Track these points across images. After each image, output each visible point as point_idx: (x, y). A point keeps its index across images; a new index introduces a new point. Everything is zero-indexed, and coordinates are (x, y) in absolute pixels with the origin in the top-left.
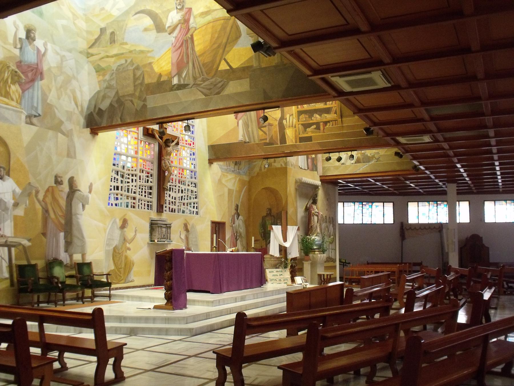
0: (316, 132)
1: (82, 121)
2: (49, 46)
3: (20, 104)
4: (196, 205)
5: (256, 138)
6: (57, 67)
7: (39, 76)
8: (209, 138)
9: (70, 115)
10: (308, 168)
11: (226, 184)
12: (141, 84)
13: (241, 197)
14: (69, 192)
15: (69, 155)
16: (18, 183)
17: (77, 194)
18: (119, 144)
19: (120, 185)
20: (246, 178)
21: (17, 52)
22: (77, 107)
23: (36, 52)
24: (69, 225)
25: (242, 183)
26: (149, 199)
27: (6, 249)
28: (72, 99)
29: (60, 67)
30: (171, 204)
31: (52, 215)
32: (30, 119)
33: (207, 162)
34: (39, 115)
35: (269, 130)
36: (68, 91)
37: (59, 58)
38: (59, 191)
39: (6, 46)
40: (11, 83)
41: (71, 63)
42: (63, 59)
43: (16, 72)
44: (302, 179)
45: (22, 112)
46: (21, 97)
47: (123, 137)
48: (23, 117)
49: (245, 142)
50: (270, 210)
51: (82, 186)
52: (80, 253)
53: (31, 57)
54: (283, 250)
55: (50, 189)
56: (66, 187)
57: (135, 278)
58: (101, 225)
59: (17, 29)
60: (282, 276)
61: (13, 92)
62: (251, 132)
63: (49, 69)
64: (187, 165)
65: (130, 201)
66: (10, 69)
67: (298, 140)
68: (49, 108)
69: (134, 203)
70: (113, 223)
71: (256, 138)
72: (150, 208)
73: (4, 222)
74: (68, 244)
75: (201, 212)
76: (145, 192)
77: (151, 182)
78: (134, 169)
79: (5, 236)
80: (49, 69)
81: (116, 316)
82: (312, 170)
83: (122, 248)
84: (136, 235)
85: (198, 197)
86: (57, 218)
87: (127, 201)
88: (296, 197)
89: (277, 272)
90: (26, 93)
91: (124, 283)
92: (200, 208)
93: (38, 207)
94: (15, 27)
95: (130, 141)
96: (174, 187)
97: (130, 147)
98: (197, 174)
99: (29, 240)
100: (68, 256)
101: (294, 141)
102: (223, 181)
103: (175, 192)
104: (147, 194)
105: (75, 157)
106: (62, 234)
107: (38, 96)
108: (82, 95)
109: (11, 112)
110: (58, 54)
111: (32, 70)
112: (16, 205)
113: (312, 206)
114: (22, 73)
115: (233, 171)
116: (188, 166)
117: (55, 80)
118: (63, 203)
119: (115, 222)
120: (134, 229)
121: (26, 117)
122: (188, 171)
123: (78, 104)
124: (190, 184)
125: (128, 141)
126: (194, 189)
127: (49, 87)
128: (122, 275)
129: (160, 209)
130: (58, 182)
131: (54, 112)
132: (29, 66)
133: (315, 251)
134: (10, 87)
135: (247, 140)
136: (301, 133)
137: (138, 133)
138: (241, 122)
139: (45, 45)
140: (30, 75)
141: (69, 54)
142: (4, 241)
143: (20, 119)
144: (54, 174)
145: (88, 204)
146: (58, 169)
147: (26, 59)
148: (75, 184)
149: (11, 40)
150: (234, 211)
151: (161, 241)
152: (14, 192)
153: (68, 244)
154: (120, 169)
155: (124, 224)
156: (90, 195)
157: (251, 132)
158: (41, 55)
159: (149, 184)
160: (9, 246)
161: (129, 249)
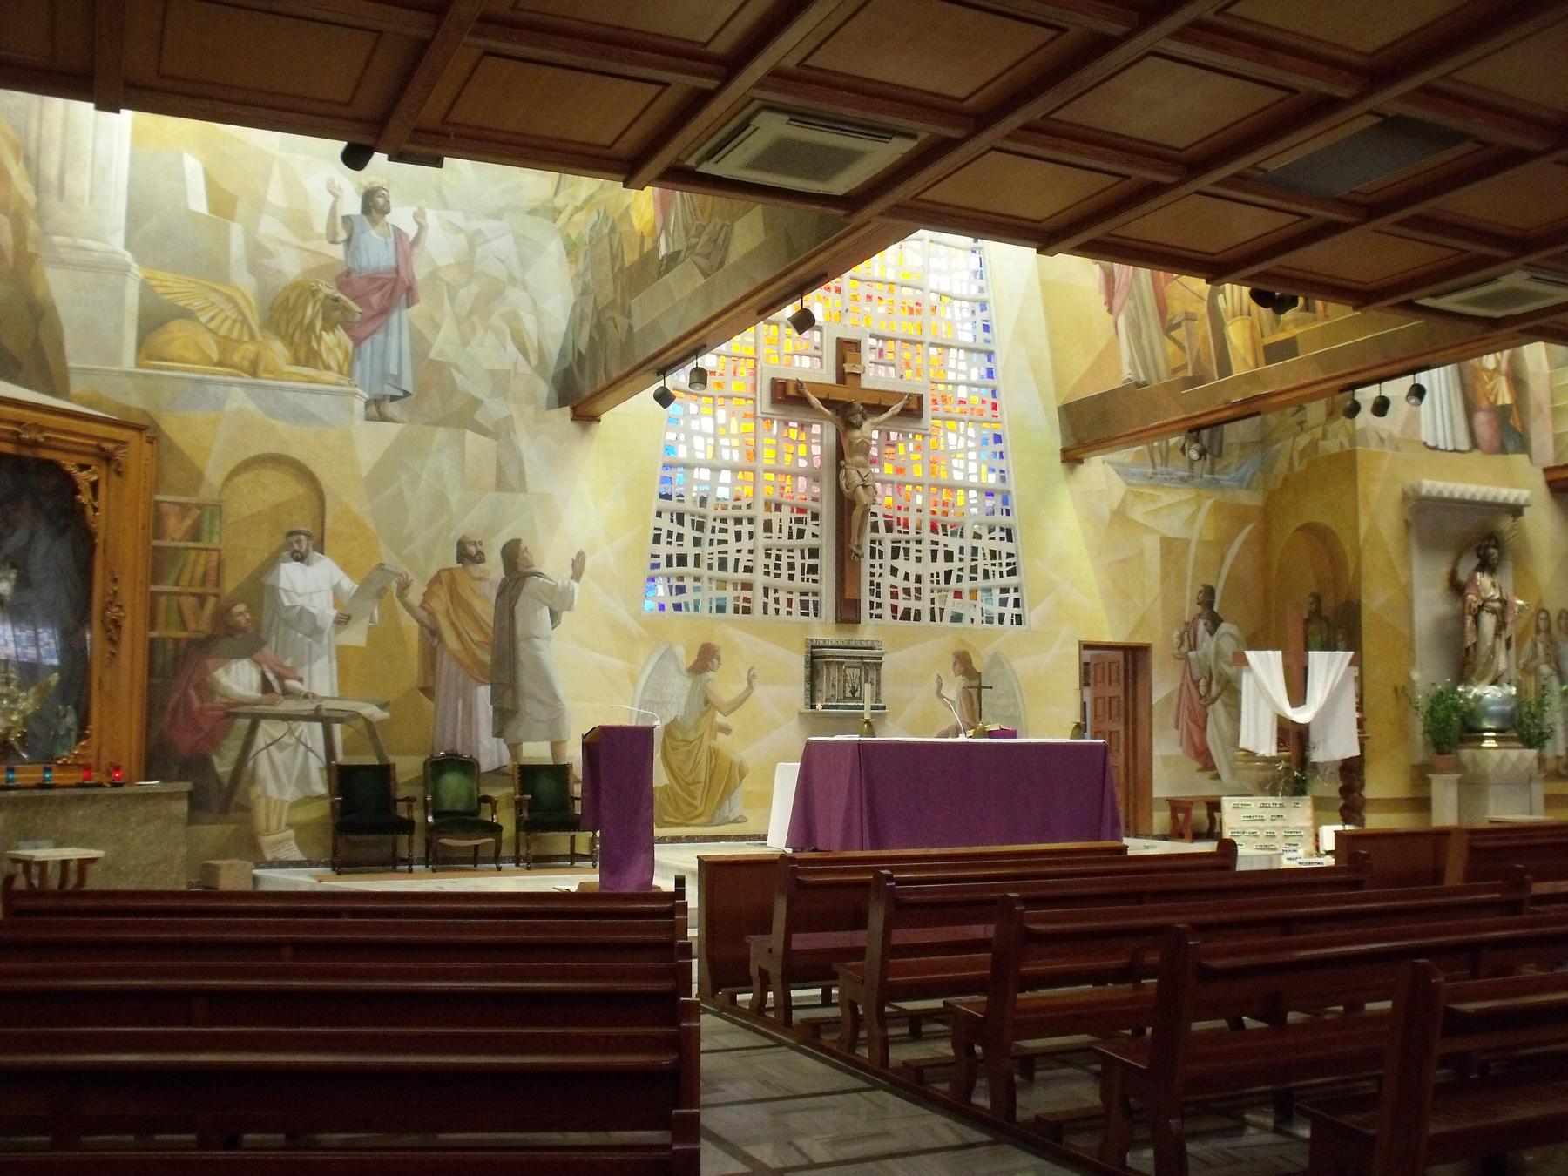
0: (1305, 322)
1: (543, 389)
2: (431, 217)
3: (350, 374)
4: (1012, 596)
5: (1162, 367)
6: (458, 264)
7: (404, 298)
8: (1058, 384)
9: (501, 382)
10: (1475, 444)
11: (1152, 524)
12: (621, 269)
13: (1229, 561)
14: (504, 581)
15: (501, 484)
16: (346, 567)
17: (532, 584)
18: (682, 437)
19: (689, 549)
20: (1251, 499)
21: (338, 252)
22: (525, 354)
23: (391, 240)
24: (506, 669)
25: (1235, 516)
26: (809, 586)
27: (318, 727)
28: (509, 338)
29: (467, 265)
30: (901, 595)
31: (451, 641)
32: (377, 409)
33: (1058, 458)
34: (406, 394)
35: (1190, 335)
36: (496, 320)
37: (462, 240)
38: (474, 579)
39: (306, 245)
40: (324, 328)
41: (504, 244)
42: (474, 240)
43: (336, 300)
44: (1420, 485)
45: (354, 394)
46: (351, 360)
47: (698, 415)
48: (359, 405)
49: (1138, 385)
50: (1317, 599)
51: (551, 562)
52: (545, 739)
53: (377, 253)
54: (1294, 737)
55: (445, 577)
56: (494, 569)
57: (745, 813)
58: (620, 664)
59: (336, 197)
60: (1278, 823)
61: (329, 349)
62: (1148, 351)
63: (434, 275)
64: (967, 475)
65: (729, 594)
66: (321, 295)
67: (1262, 359)
68: (434, 375)
69: (746, 600)
70: (663, 656)
71: (1162, 367)
72: (811, 611)
73: (310, 662)
74: (505, 718)
75: (1031, 617)
76: (791, 566)
77: (814, 535)
78: (743, 503)
79: (314, 696)
80: (434, 275)
81: (772, 915)
82: (1503, 450)
83: (696, 728)
84: (750, 687)
85: (1021, 569)
86: (467, 649)
87: (722, 594)
88: (1406, 554)
89: (1264, 806)
90: (367, 347)
91: (709, 824)
92: (1025, 602)
93: (410, 625)
94: (333, 194)
95: (726, 426)
96: (913, 546)
97: (724, 442)
98: (1014, 504)
99: (383, 706)
100: (504, 747)
101: (1250, 361)
102: (1138, 513)
103: (918, 559)
104: (797, 572)
105: (523, 488)
106: (484, 693)
107: (400, 348)
108: (539, 321)
109: (323, 398)
110: (458, 230)
111: (382, 287)
112: (343, 621)
113: (1472, 579)
114: (354, 299)
115: (1183, 480)
116: (973, 479)
117: (452, 299)
118: (485, 608)
119: (668, 654)
120: (745, 675)
121: (367, 404)
122: (973, 494)
123: (529, 346)
124: (984, 531)
125: (716, 426)
126: (1006, 547)
127: (433, 320)
128: (697, 803)
129: (848, 612)
130: (468, 554)
131: (453, 381)
132: (372, 279)
133: (1483, 739)
134: (319, 339)
135: (1143, 378)
136: (1267, 330)
137: (754, 400)
138: (1122, 320)
139: (419, 218)
140: (375, 299)
141: (494, 224)
142: (313, 706)
143: (351, 411)
144: (455, 535)
145: (570, 607)
146: (467, 525)
147: (364, 263)
148: (525, 559)
149: (320, 227)
150: (1189, 607)
151: (836, 707)
152: (336, 590)
153: (505, 718)
154: (689, 505)
155: (706, 658)
156: (576, 586)
157: (1148, 351)
158: (405, 246)
159: (808, 540)
160: (326, 720)
161: (726, 730)
